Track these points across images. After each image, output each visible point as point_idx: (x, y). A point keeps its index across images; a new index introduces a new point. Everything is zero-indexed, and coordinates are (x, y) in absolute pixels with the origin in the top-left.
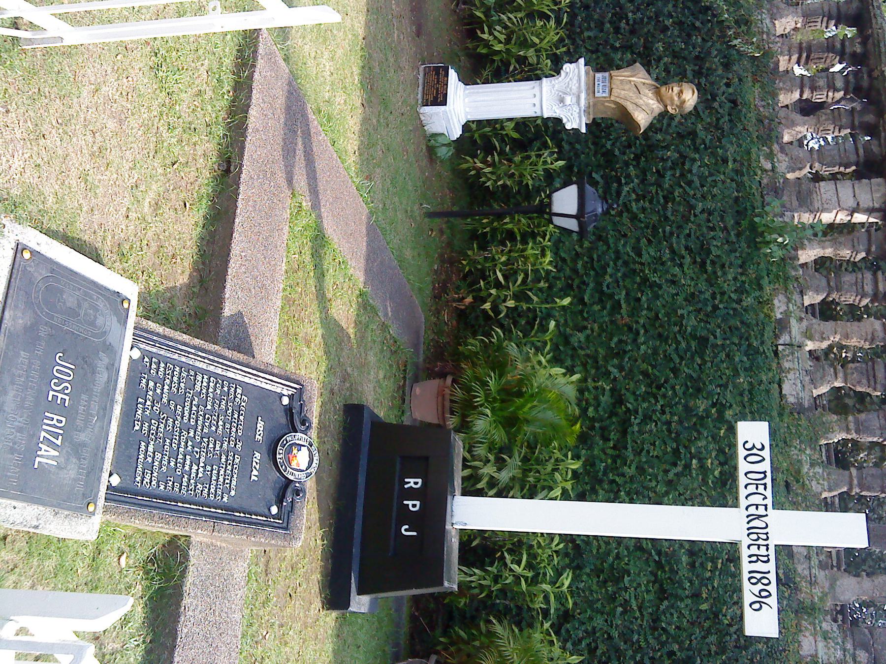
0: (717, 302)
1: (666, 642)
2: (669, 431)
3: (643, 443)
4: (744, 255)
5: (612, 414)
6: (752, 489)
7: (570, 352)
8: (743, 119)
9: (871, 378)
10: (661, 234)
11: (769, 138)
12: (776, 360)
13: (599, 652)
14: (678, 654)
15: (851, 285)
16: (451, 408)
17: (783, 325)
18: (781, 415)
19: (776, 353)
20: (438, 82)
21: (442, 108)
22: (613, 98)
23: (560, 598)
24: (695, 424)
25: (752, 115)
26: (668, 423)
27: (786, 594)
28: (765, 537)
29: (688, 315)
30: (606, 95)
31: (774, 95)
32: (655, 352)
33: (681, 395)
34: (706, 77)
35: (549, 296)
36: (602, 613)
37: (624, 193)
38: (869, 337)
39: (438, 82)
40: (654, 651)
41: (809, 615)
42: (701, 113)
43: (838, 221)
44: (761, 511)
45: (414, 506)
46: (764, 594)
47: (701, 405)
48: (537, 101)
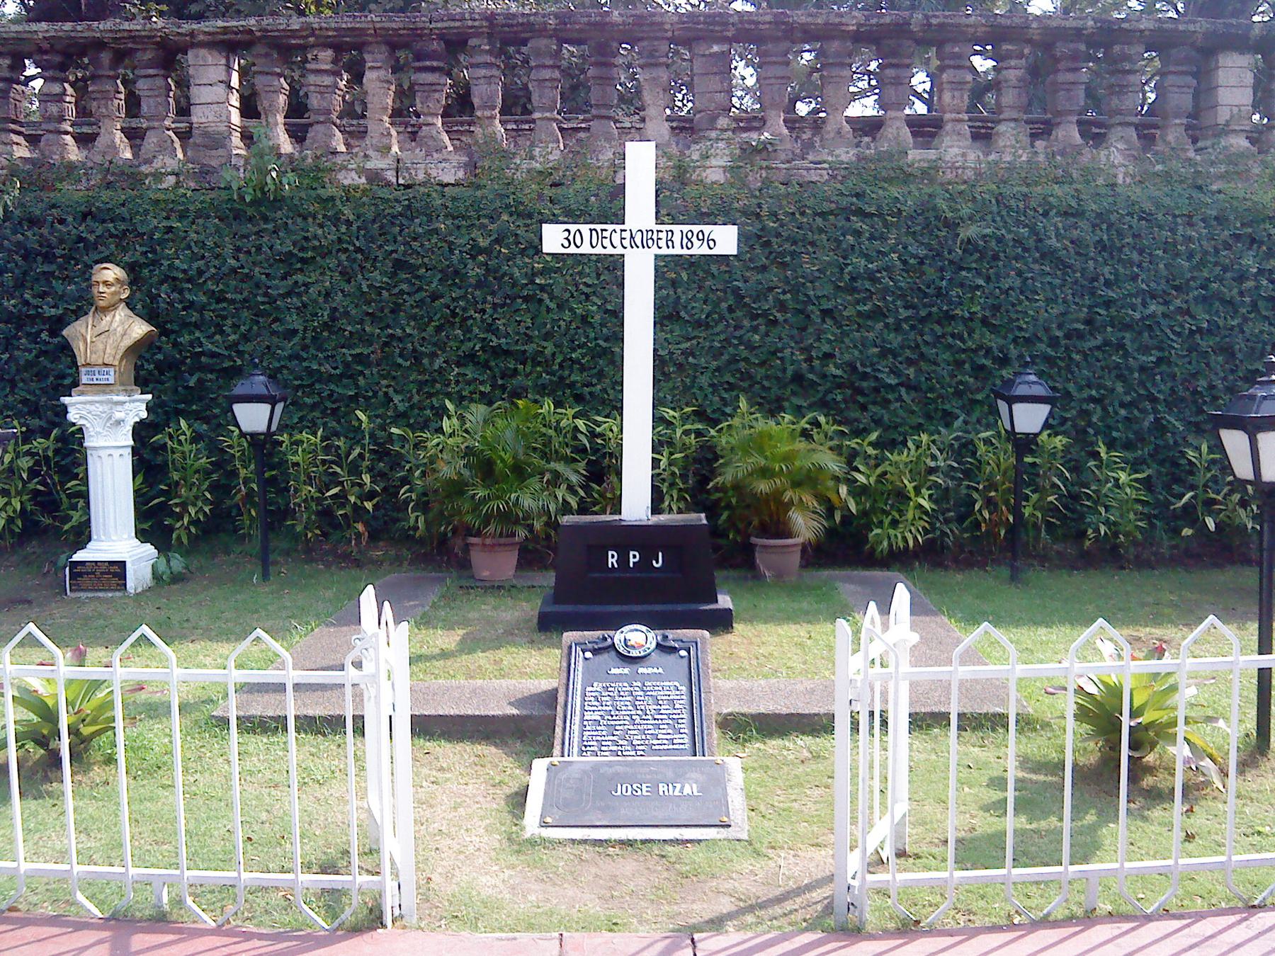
0: (351, 248)
1: (719, 314)
2: (503, 306)
3: (518, 333)
4: (291, 214)
5: (486, 366)
6: (607, 243)
7: (416, 411)
8: (108, 206)
9: (434, 88)
10: (267, 306)
11: (132, 176)
12: (417, 187)
13: (732, 380)
14: (730, 302)
15: (323, 98)
16: (508, 536)
17: (375, 177)
18: (479, 187)
19: (407, 187)
20: (93, 573)
21: (128, 566)
22: (116, 363)
23: (685, 419)
24: (495, 279)
25: (106, 195)
26: (495, 306)
27: (668, 193)
28: (650, 233)
29: (368, 280)
30: (112, 370)
31: (71, 167)
32: (414, 317)
33: (463, 291)
34: (53, 248)
35: (355, 433)
36: (695, 377)
37: (214, 349)
38: (386, 85)
39: (93, 573)
40: (728, 326)
41: (685, 171)
42: (102, 255)
43: (237, 104)
44: (627, 235)
45: (634, 556)
46: (701, 237)
47: (474, 272)
48: (116, 453)
